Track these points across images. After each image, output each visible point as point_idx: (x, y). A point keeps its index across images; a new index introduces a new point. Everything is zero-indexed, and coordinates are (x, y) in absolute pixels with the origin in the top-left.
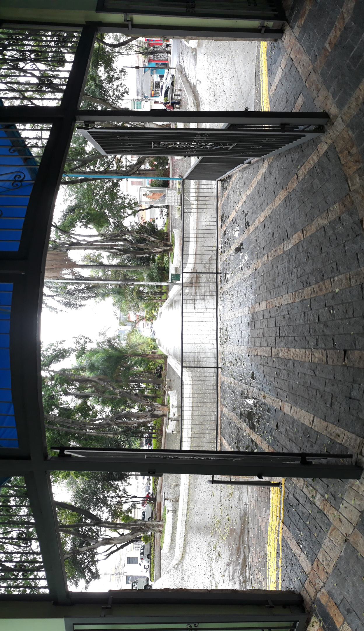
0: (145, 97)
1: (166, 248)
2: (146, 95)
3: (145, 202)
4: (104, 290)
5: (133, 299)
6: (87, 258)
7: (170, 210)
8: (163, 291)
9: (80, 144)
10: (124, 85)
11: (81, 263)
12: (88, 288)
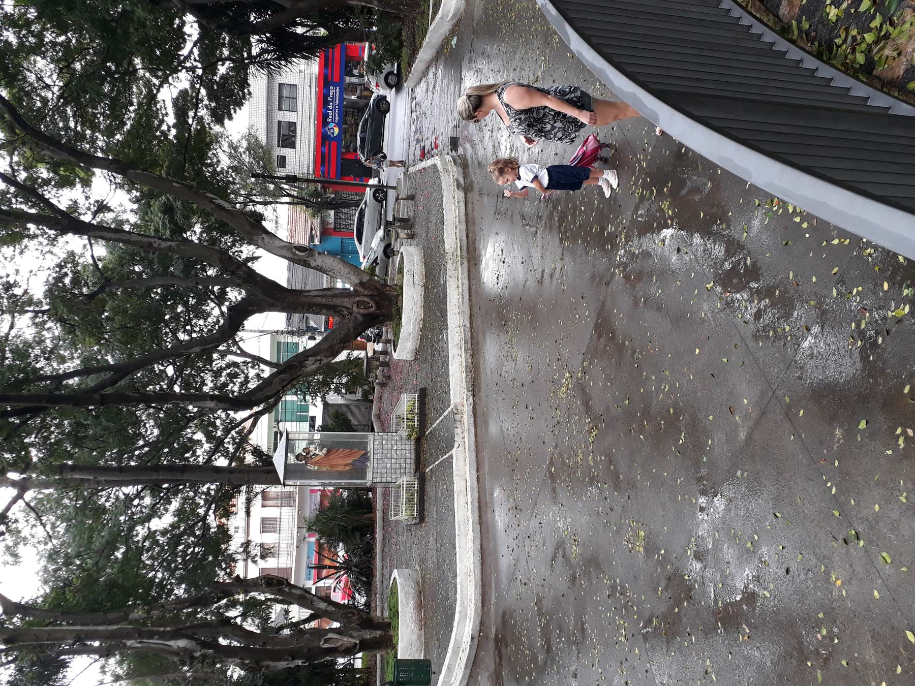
1: (368, 635)
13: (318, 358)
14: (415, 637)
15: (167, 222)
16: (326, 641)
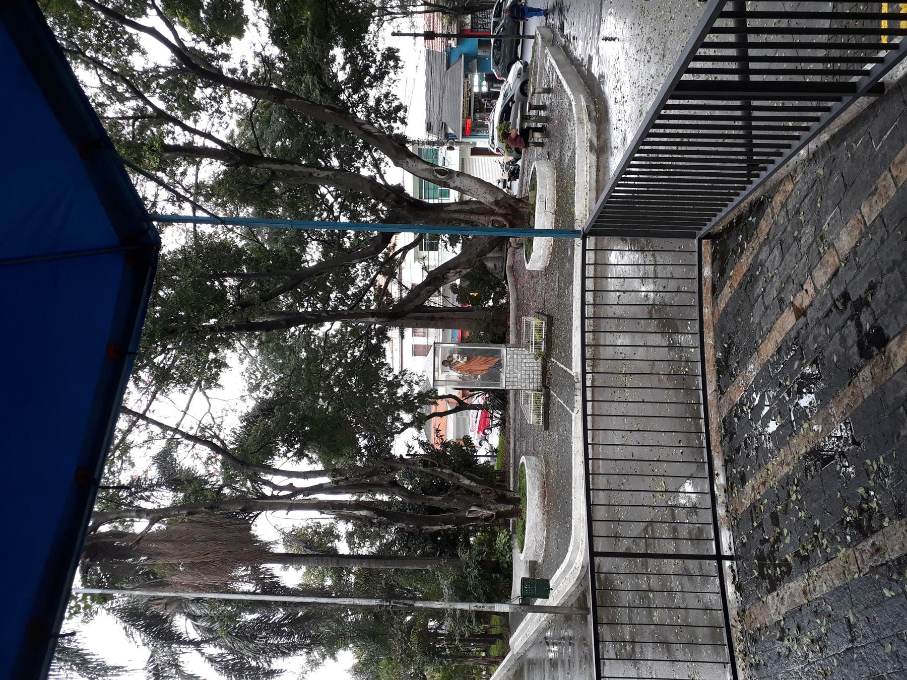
0: (447, 135)
1: (502, 508)
2: (450, 131)
3: (448, 384)
4: (334, 625)
5: (410, 655)
6: (291, 537)
7: (511, 412)
8: (494, 631)
9: (286, 244)
10: (395, 98)
11: (280, 549)
12: (295, 623)
13: (458, 270)
14: (539, 520)
15: (316, 82)
16: (470, 512)
